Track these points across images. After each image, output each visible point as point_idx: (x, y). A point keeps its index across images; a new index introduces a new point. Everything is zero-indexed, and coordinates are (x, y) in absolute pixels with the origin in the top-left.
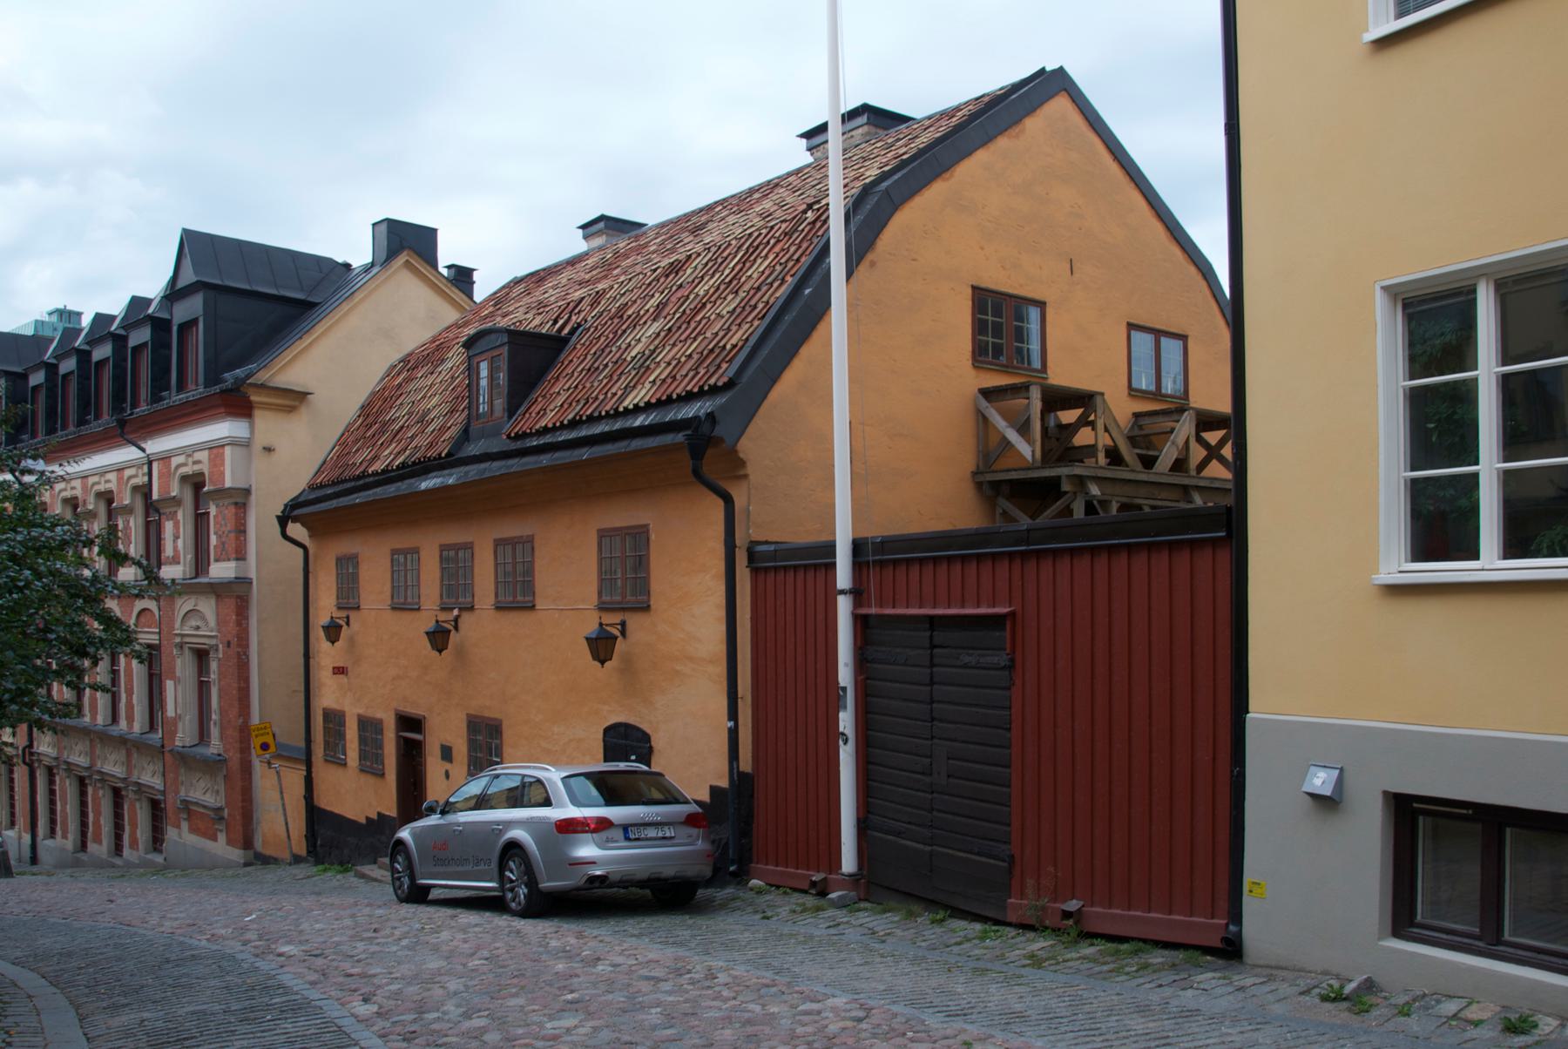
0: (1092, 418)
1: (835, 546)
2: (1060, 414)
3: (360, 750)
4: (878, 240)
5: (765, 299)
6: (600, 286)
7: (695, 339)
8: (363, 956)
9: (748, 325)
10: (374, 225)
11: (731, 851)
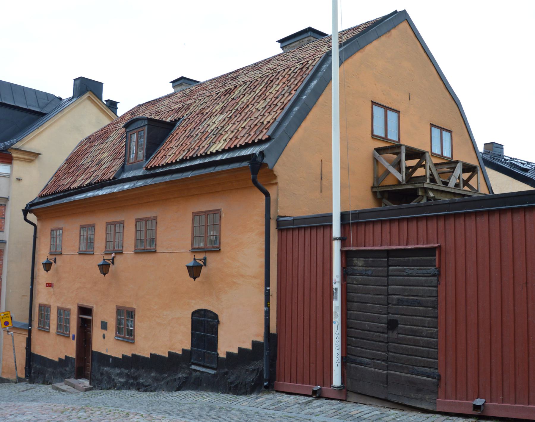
0: (424, 163)
1: (332, 216)
3: (58, 324)
5: (282, 101)
7: (245, 120)
10: (75, 80)
11: (265, 375)
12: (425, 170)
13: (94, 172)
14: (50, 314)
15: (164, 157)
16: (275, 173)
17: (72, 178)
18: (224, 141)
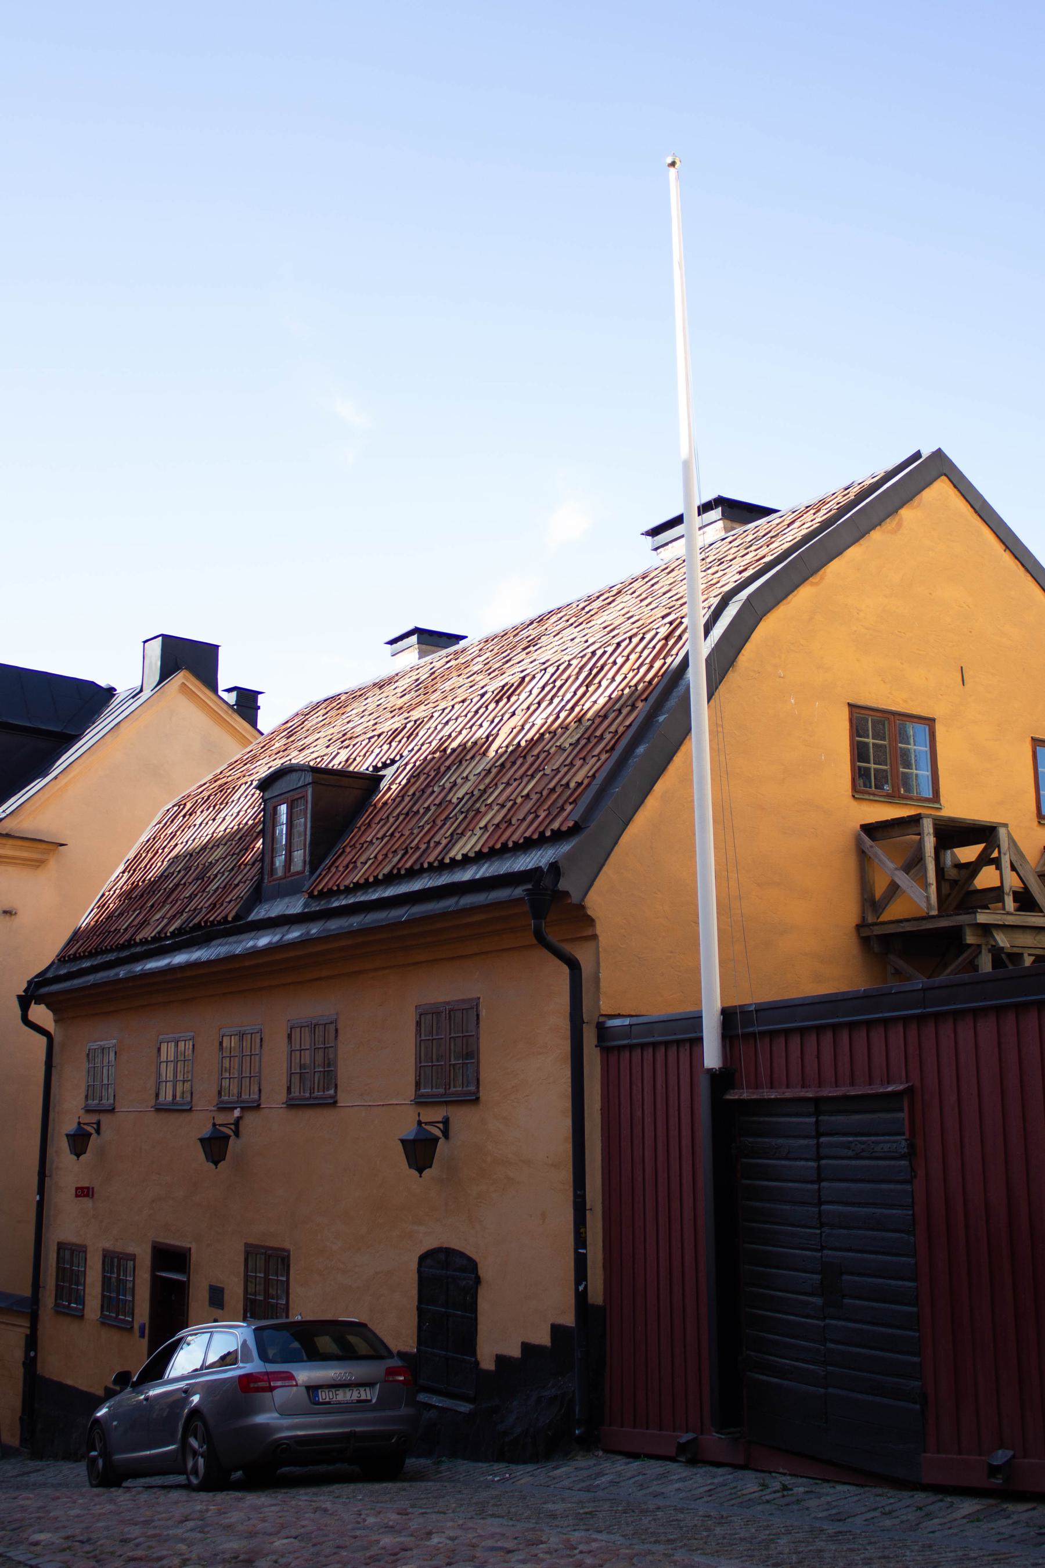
0: (995, 854)
2: (956, 850)
3: (103, 1296)
4: (740, 655)
5: (613, 729)
6: (416, 714)
7: (532, 776)
8: (141, 1540)
9: (595, 759)
12: (998, 871)
13: (191, 898)
14: (85, 1271)
15: (351, 866)
16: (589, 912)
17: (138, 912)
18: (482, 831)
